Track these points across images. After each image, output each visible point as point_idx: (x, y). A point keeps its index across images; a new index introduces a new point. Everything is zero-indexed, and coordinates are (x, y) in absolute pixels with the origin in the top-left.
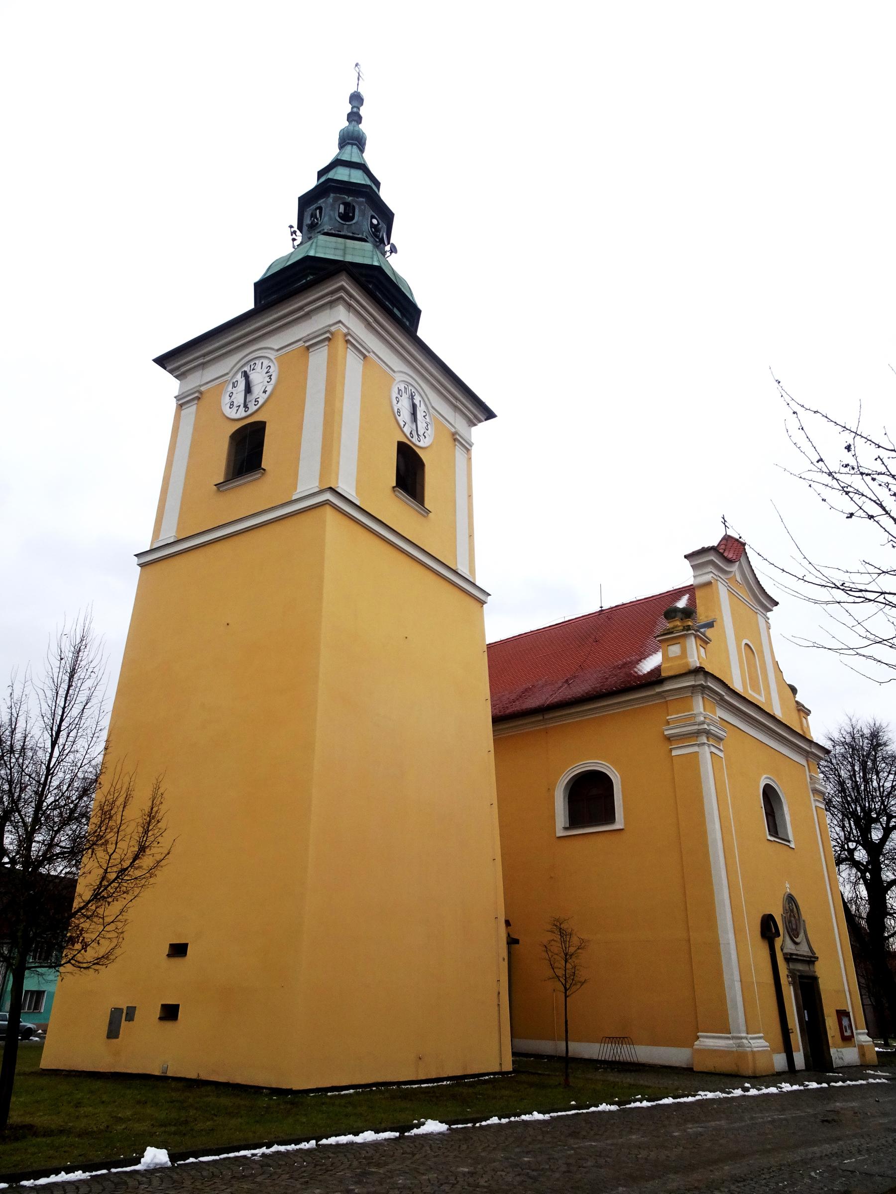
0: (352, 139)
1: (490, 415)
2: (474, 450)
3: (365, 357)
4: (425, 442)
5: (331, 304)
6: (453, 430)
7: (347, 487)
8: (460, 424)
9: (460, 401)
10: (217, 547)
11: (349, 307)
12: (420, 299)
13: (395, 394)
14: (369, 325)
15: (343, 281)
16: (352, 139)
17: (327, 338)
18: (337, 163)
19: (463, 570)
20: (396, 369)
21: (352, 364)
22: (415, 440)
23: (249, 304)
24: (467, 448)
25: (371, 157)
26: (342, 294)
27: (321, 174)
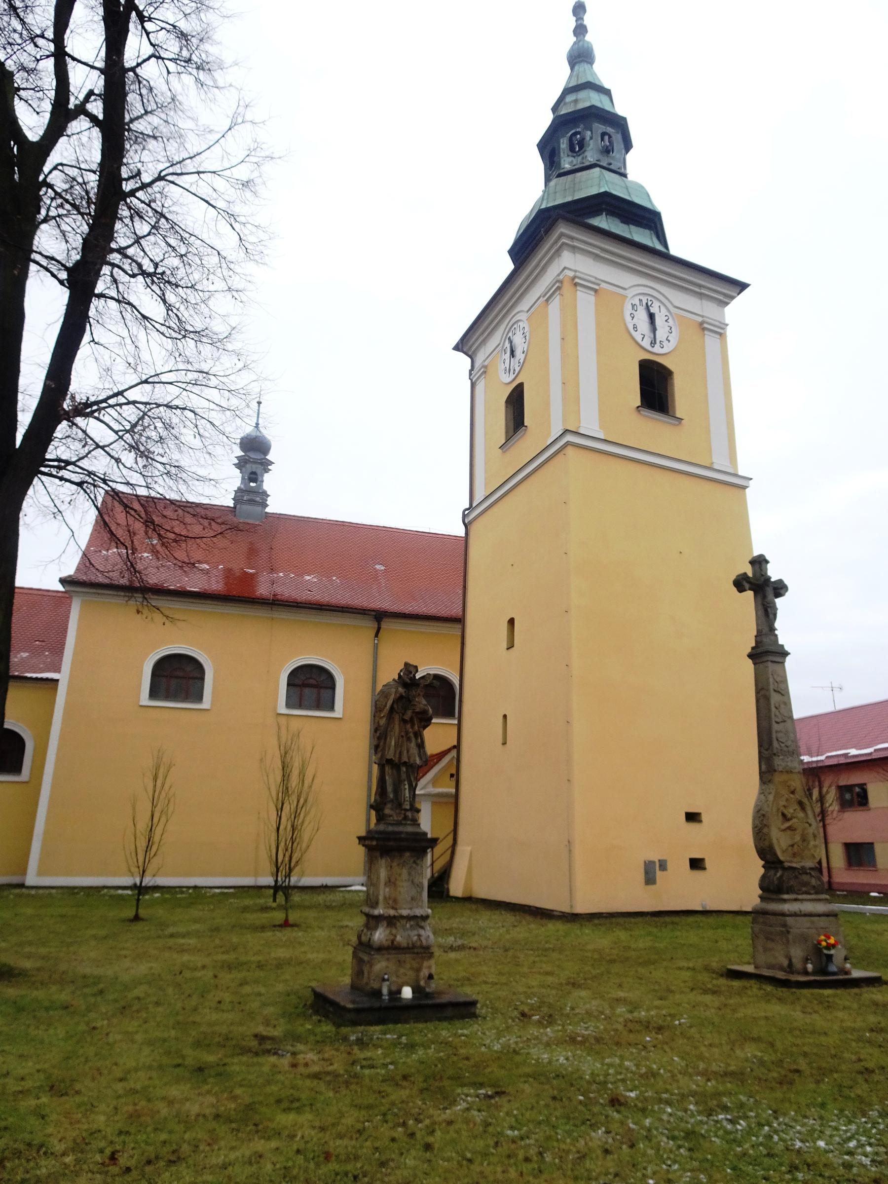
0: (580, 56)
1: (742, 286)
2: (730, 332)
3: (596, 291)
4: (667, 348)
5: (558, 253)
6: (700, 319)
7: (590, 424)
8: (708, 309)
9: (578, 239)
10: (490, 512)
11: (574, 249)
12: (659, 203)
13: (628, 309)
14: (597, 257)
15: (563, 229)
16: (580, 56)
17: (557, 287)
18: (567, 91)
19: (720, 462)
20: (626, 287)
21: (585, 301)
22: (657, 349)
23: (510, 266)
24: (720, 331)
25: (603, 71)
26: (564, 240)
27: (555, 109)
